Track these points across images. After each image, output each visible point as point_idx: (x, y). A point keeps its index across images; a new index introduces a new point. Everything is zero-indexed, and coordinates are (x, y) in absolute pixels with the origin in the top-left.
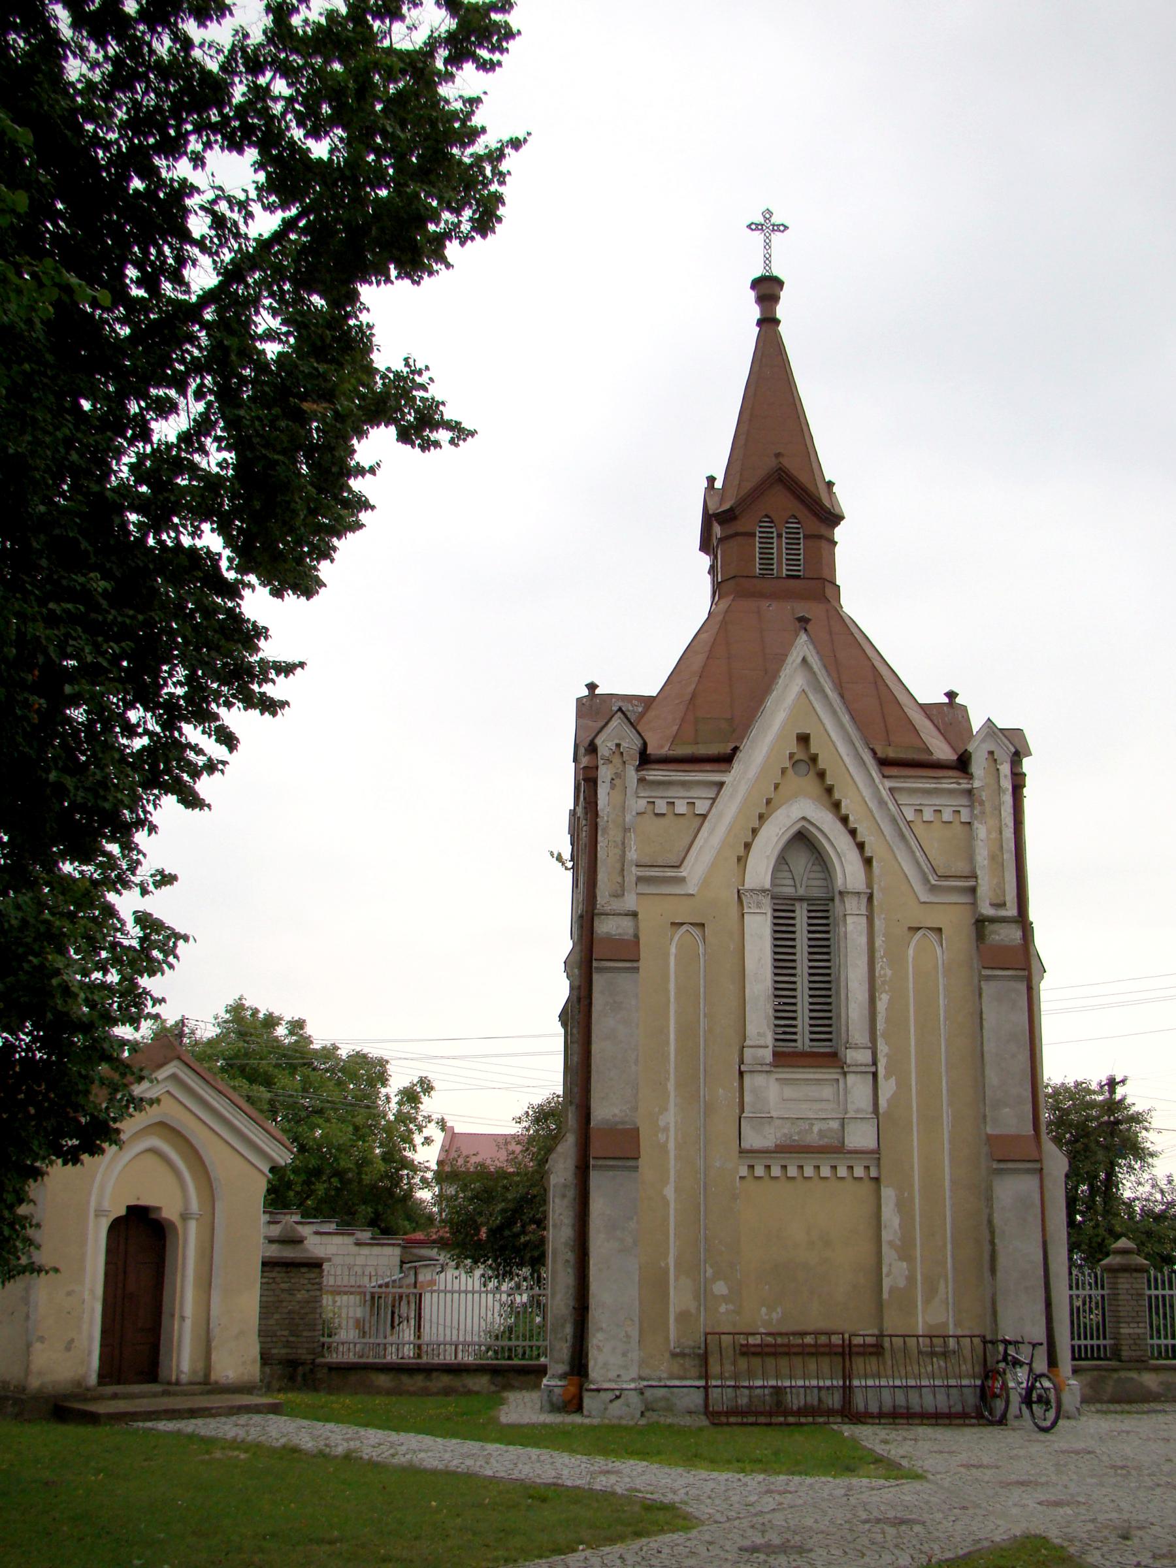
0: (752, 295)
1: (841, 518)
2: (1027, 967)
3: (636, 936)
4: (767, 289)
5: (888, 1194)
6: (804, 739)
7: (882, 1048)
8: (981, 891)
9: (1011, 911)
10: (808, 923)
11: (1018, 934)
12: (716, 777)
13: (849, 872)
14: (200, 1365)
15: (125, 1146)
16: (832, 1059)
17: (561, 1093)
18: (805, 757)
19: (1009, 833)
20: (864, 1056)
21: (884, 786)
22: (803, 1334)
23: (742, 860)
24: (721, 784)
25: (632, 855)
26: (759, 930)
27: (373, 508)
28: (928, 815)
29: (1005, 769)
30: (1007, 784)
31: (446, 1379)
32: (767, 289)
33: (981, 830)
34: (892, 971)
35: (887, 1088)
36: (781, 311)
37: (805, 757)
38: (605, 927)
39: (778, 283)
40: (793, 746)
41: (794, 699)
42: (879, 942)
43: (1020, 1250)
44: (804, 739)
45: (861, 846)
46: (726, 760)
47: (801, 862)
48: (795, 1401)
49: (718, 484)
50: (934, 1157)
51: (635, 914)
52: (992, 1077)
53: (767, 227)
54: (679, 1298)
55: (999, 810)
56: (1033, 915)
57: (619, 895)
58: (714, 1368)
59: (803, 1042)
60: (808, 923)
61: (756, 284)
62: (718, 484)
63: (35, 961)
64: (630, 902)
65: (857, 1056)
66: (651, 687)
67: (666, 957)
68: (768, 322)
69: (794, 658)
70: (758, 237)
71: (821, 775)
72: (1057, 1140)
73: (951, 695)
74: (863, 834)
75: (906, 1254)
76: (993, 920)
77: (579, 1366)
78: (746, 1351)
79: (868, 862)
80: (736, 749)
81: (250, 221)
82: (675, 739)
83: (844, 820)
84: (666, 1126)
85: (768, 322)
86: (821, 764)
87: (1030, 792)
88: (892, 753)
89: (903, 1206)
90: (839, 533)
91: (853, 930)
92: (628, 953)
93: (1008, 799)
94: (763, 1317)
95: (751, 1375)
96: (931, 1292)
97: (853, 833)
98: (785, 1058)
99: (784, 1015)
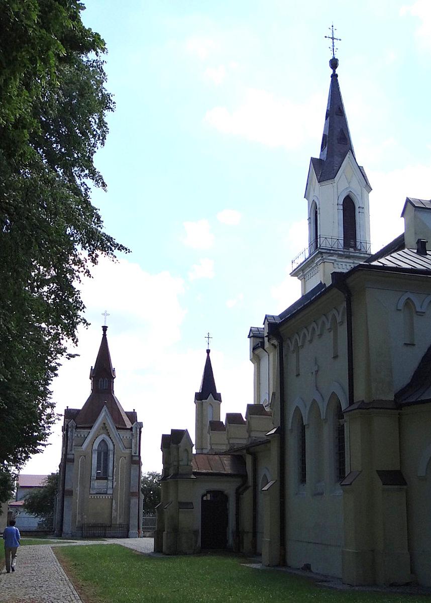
2: (139, 464)
3: (74, 459)
5: (114, 501)
6: (104, 424)
7: (114, 477)
8: (133, 451)
9: (137, 454)
10: (104, 454)
11: (138, 458)
12: (89, 431)
13: (111, 447)
15: (379, 483)
16: (106, 479)
17: (161, 474)
19: (138, 441)
20: (112, 478)
22: (98, 524)
23: (93, 445)
25: (74, 444)
26: (95, 456)
28: (125, 438)
29: (138, 430)
30: (138, 433)
31: (35, 533)
33: (133, 441)
34: (117, 464)
35: (115, 484)
37: (104, 427)
38: (69, 456)
40: (102, 425)
41: (104, 415)
42: (115, 459)
43: (134, 511)
45: (113, 443)
47: (103, 444)
48: (97, 535)
49: (93, 368)
50: (121, 495)
51: (74, 454)
52: (132, 482)
53: (106, 314)
54: (78, 518)
55: (136, 437)
56: (141, 455)
57: (71, 450)
58: (84, 530)
60: (104, 454)
64: (73, 452)
65: (110, 478)
66: (80, 407)
67: (79, 462)
68: (105, 335)
69: (103, 410)
70: (104, 317)
71: (107, 430)
72: (143, 493)
74: (113, 441)
75: (116, 511)
76: (134, 456)
77: (61, 530)
78: (89, 527)
79: (114, 445)
81: (50, 428)
83: (110, 438)
84: (78, 490)
85: (105, 335)
86: (107, 428)
87: (142, 434)
89: (116, 503)
91: (111, 456)
92: (72, 461)
93: (138, 435)
94: (92, 521)
95: (89, 531)
96: (120, 518)
97: (112, 440)
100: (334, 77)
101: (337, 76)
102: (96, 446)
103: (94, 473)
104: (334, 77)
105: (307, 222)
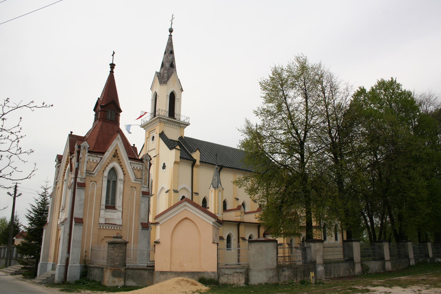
0: (109, 66)
1: (121, 111)
4: (112, 66)
12: (101, 156)
13: (121, 175)
14: (62, 276)
15: (140, 227)
18: (116, 155)
21: (129, 161)
24: (102, 158)
27: (163, 132)
32: (112, 66)
36: (114, 70)
39: (115, 65)
44: (116, 150)
46: (103, 153)
59: (110, 205)
61: (110, 64)
62: (100, 99)
63: (288, 204)
68: (112, 72)
73: (134, 145)
80: (105, 152)
82: (94, 148)
85: (112, 72)
88: (131, 157)
90: (121, 114)
98: (107, 207)
99: (107, 201)
100: (171, 36)
101: (171, 36)
102: (106, 174)
103: (104, 202)
104: (171, 36)
105: (151, 101)
